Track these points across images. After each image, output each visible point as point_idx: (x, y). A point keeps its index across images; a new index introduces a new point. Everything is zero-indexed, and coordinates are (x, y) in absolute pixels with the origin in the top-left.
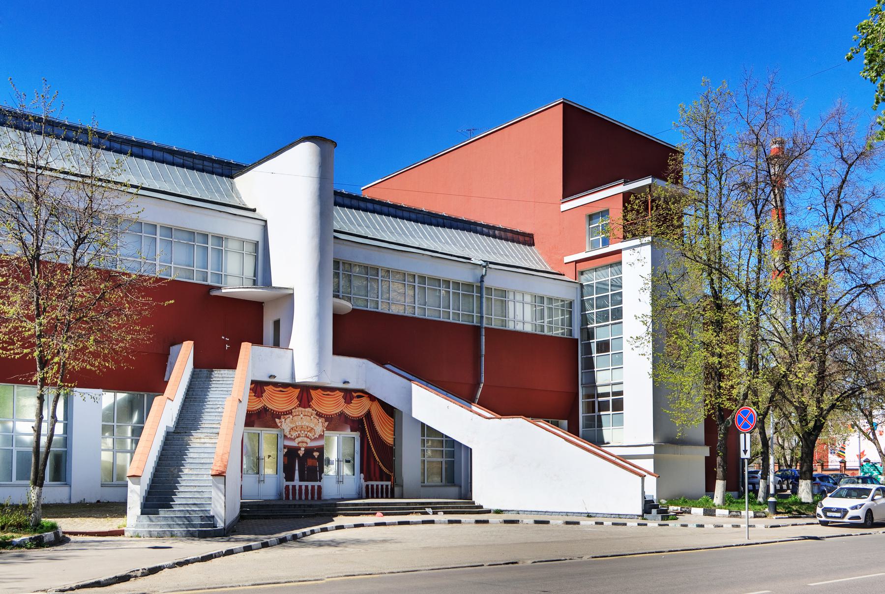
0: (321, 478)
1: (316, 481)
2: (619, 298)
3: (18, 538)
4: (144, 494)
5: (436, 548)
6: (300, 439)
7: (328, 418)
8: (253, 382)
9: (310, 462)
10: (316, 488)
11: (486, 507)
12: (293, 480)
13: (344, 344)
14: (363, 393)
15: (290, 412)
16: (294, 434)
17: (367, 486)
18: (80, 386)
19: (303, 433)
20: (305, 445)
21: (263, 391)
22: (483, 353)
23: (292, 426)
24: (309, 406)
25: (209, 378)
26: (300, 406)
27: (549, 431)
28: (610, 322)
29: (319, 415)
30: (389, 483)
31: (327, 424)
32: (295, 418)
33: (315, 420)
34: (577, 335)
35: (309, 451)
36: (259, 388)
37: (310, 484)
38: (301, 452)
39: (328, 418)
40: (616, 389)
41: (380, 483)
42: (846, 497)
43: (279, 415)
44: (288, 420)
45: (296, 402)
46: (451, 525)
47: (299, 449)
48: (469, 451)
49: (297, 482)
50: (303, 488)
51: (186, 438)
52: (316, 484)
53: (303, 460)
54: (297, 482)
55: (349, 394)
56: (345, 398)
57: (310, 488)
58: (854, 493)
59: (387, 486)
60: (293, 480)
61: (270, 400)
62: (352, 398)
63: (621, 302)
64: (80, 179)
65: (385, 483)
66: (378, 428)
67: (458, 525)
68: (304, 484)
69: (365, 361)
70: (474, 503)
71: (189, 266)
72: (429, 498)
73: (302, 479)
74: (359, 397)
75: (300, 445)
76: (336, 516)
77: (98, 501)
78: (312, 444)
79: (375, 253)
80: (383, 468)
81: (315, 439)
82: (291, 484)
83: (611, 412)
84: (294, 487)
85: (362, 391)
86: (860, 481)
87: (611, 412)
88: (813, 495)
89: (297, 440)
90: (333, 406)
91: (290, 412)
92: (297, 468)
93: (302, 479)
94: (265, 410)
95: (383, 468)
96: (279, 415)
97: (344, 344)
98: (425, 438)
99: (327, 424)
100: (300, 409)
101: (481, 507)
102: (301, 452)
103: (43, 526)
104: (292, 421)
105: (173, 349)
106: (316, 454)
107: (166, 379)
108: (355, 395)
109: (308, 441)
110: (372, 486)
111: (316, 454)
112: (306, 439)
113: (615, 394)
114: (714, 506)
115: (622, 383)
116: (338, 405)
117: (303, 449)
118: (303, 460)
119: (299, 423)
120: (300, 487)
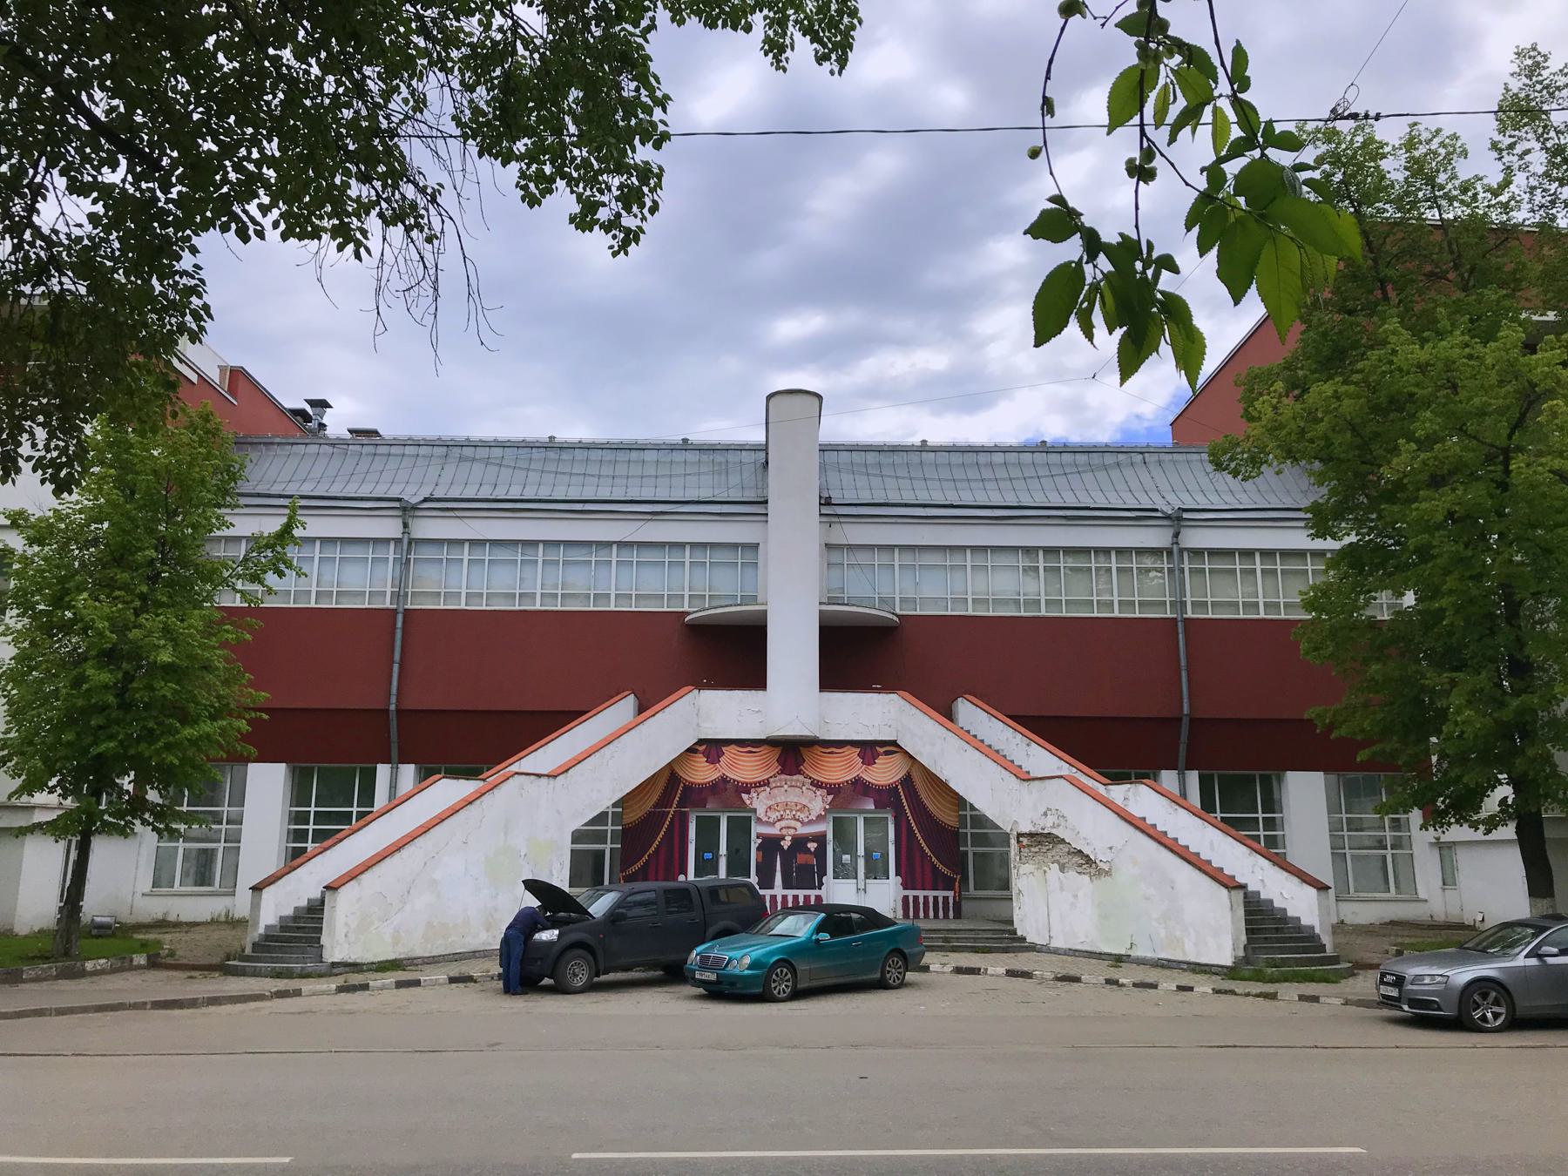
0: (821, 884)
2: (783, 988)
4: (289, 912)
6: (783, 824)
8: (509, 990)
9: (801, 858)
14: (892, 747)
15: (766, 783)
16: (774, 816)
20: (792, 832)
23: (770, 803)
24: (799, 772)
25: (1280, 780)
26: (783, 772)
29: (817, 785)
30: (950, 894)
34: (10, 638)
35: (800, 842)
36: (713, 751)
43: (747, 788)
46: (403, 991)
49: (778, 890)
51: (203, 358)
53: (788, 856)
54: (778, 890)
55: (869, 750)
58: (1490, 1013)
59: (946, 899)
62: (875, 756)
64: (1155, 537)
65: (941, 894)
66: (931, 807)
67: (414, 990)
68: (790, 893)
70: (1015, 932)
71: (983, 855)
72: (391, 676)
74: (887, 753)
75: (784, 832)
78: (803, 830)
79: (994, 904)
80: (938, 865)
81: (811, 822)
84: (774, 898)
85: (894, 743)
88: (636, 63)
89: (779, 825)
90: (840, 770)
91: (766, 783)
92: (221, 1160)
95: (938, 865)
96: (747, 788)
101: (1023, 939)
102: (786, 844)
103: (1291, 455)
106: (812, 846)
107: (194, 378)
108: (881, 750)
109: (798, 825)
111: (812, 846)
112: (793, 823)
116: (851, 767)
117: (789, 838)
118: (788, 856)
120: (785, 898)
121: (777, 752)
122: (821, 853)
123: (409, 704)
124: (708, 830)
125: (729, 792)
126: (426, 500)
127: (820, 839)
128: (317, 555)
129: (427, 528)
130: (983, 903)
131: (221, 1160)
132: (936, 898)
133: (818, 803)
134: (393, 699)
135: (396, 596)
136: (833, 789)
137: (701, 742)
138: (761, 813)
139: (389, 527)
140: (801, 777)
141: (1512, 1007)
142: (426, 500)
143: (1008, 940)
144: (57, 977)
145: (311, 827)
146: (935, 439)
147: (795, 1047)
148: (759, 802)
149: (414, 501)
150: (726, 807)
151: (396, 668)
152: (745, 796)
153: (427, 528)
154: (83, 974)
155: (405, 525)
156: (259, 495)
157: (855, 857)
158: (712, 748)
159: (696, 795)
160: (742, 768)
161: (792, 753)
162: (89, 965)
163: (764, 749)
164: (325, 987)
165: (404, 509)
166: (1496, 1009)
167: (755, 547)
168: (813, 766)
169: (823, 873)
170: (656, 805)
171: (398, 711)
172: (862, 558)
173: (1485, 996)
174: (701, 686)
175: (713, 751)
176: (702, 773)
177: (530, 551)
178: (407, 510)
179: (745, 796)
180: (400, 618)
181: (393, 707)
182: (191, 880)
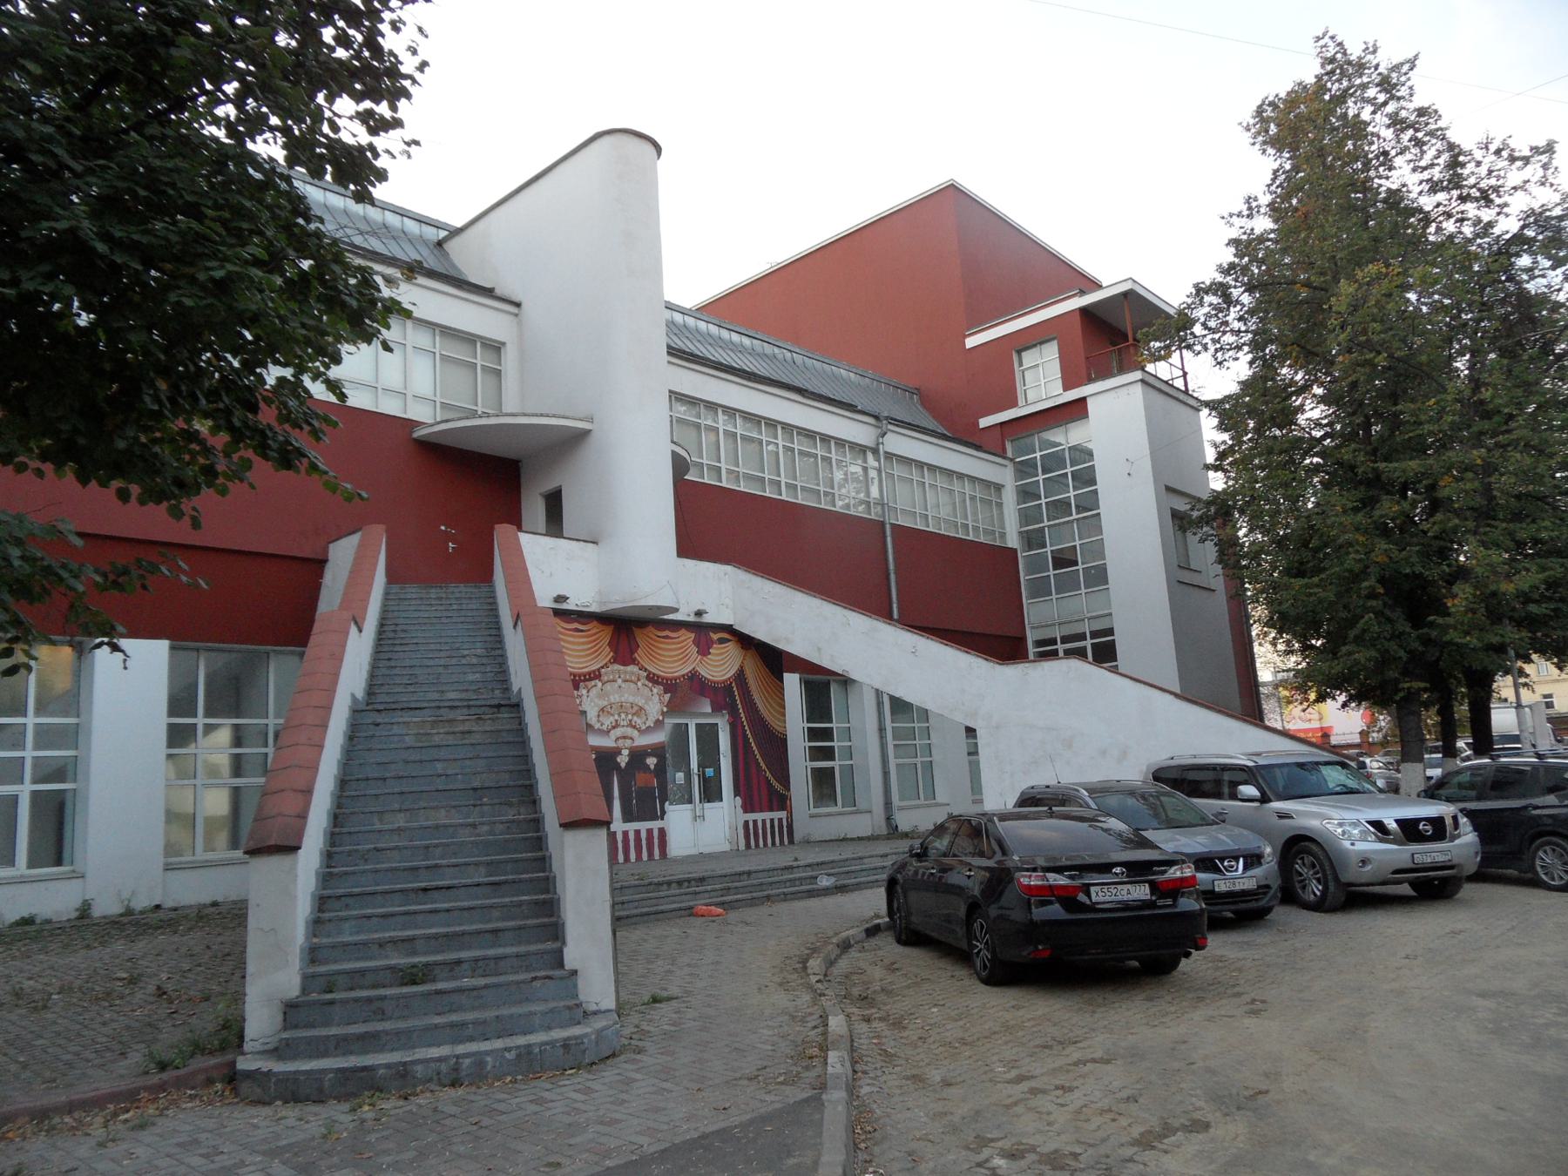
1: (654, 817)
5: (869, 839)
6: (618, 732)
7: (669, 686)
11: (459, 225)
13: (692, 543)
15: (596, 675)
16: (608, 721)
17: (746, 823)
19: (624, 719)
20: (628, 743)
22: (892, 567)
24: (633, 661)
26: (615, 660)
27: (1218, 756)
28: (1075, 516)
29: (653, 679)
30: (783, 815)
31: (667, 697)
32: (608, 687)
33: (646, 691)
37: (643, 826)
39: (669, 686)
40: (1098, 626)
41: (767, 815)
42: (613, 916)
44: (594, 692)
45: (607, 654)
47: (618, 752)
48: (952, 193)
50: (632, 836)
52: (655, 825)
55: (704, 632)
56: (697, 642)
57: (644, 835)
63: (1093, 482)
69: (729, 568)
74: (721, 641)
75: (620, 743)
77: (129, 912)
80: (773, 781)
85: (728, 629)
87: (1083, 591)
90: (677, 658)
91: (596, 675)
95: (773, 781)
97: (692, 543)
99: (667, 697)
100: (617, 667)
102: (623, 760)
105: (331, 546)
108: (715, 637)
111: (651, 762)
112: (630, 731)
113: (1094, 634)
114: (1316, 380)
117: (625, 752)
119: (615, 698)
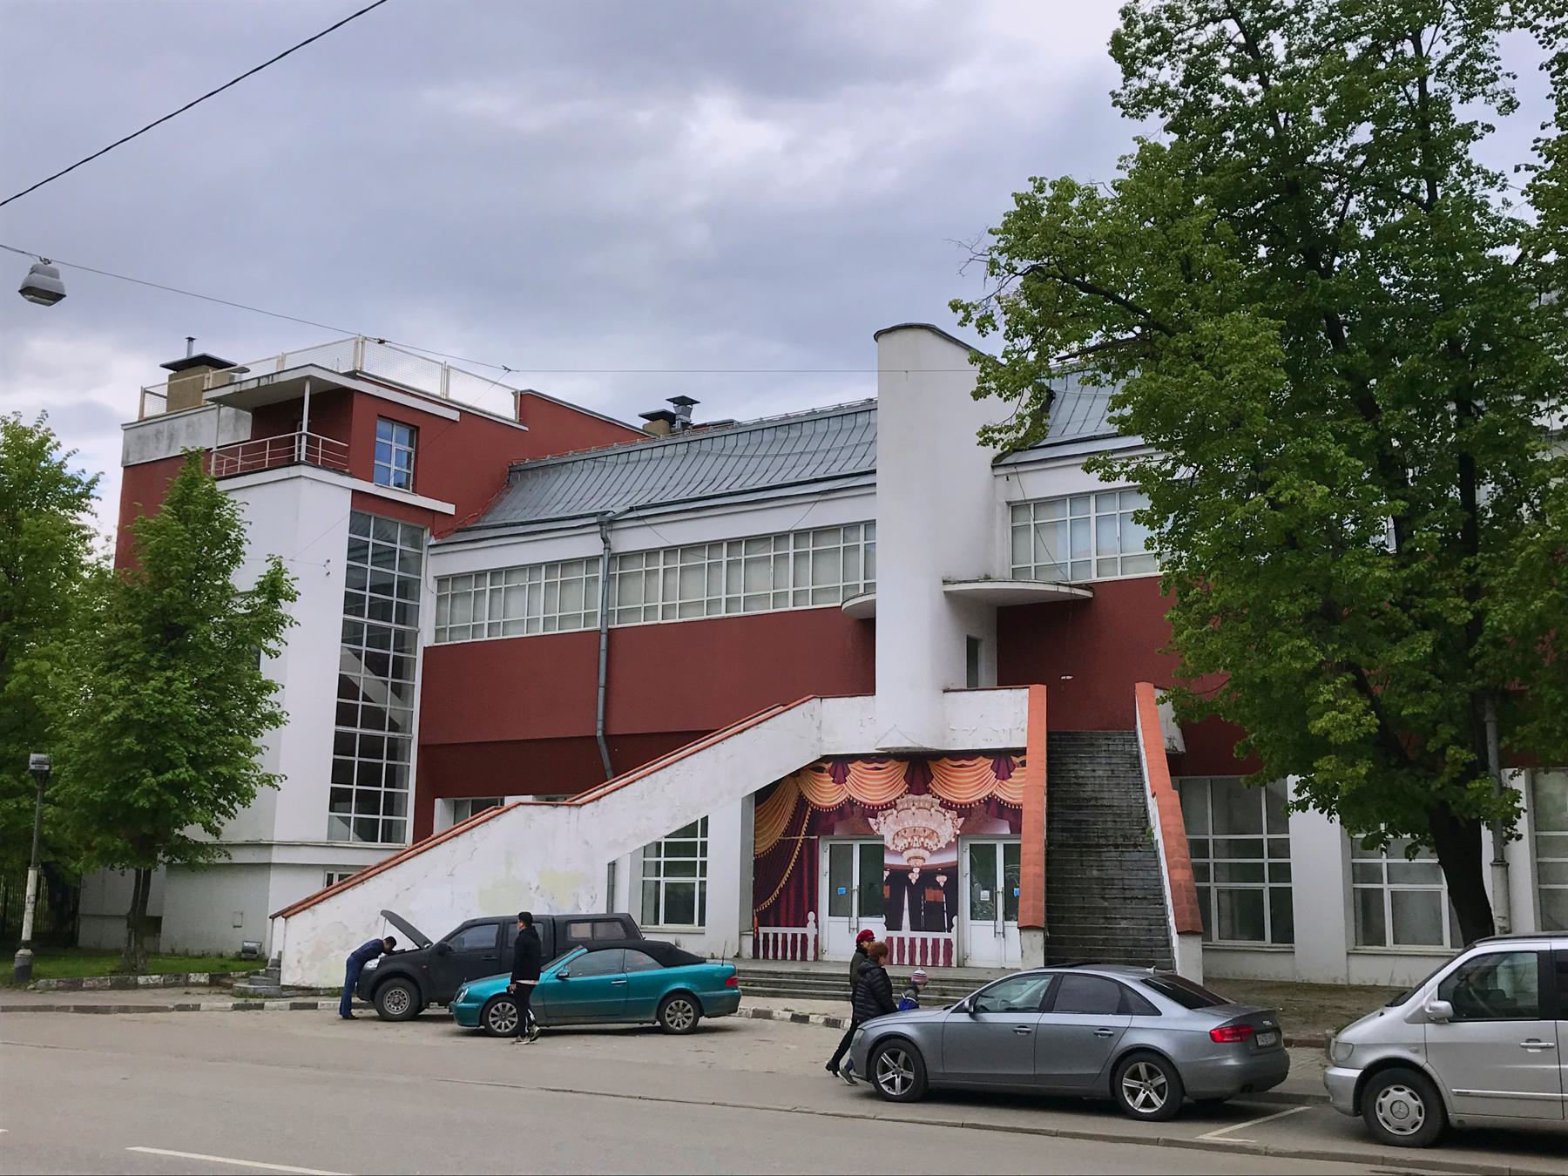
0: (951, 925)
1: (942, 930)
2: (506, 1025)
3: (1293, 1020)
6: (911, 853)
9: (930, 895)
10: (942, 943)
12: (899, 929)
15: (892, 805)
16: (901, 843)
18: (1048, 942)
19: (916, 842)
20: (920, 863)
21: (846, 772)
24: (928, 791)
26: (909, 791)
29: (947, 805)
35: (928, 875)
36: (1003, 763)
37: (930, 936)
38: (914, 877)
43: (873, 811)
44: (890, 819)
49: (906, 932)
54: (906, 932)
60: (899, 929)
61: (858, 787)
63: (339, 736)
68: (919, 935)
73: (915, 927)
75: (912, 863)
76: (1349, 825)
79: (1249, 958)
81: (940, 851)
82: (895, 934)
83: (664, 841)
86: (842, 890)
89: (907, 854)
90: (971, 786)
91: (892, 805)
93: (915, 927)
94: (851, 802)
96: (873, 811)
98: (698, 859)
100: (911, 796)
102: (914, 877)
104: (898, 820)
106: (942, 880)
107: (455, 416)
109: (926, 854)
110: (923, 964)
111: (942, 880)
112: (922, 852)
115: (874, 472)
116: (983, 783)
117: (917, 870)
118: (917, 891)
119: (909, 823)
121: (903, 768)
122: (952, 888)
123: (616, 730)
124: (840, 858)
125: (856, 815)
126: (631, 510)
127: (952, 871)
128: (1093, 515)
129: (629, 540)
130: (1236, 956)
131: (203, 1157)
132: (924, 941)
133: (947, 827)
134: (600, 725)
135: (607, 615)
136: (964, 811)
137: (826, 759)
138: (888, 841)
139: (591, 545)
140: (928, 797)
141: (922, 1072)
142: (631, 510)
143: (78, 948)
144: (112, 988)
145: (1266, 861)
146: (745, 414)
147: (214, 1060)
148: (886, 827)
149: (617, 510)
150: (856, 835)
151: (601, 691)
152: (871, 820)
153: (629, 540)
154: (136, 986)
155: (605, 541)
156: (506, 525)
157: (993, 896)
158: (838, 765)
159: (823, 821)
160: (869, 787)
161: (919, 768)
162: (141, 980)
163: (890, 765)
164: (221, 1005)
165: (601, 524)
166: (1154, 1097)
167: (870, 524)
168: (945, 785)
169: (954, 910)
170: (784, 834)
171: (606, 737)
172: (1065, 513)
173: (1152, 1073)
174: (824, 694)
175: (1003, 763)
176: (827, 794)
177: (1079, 506)
178: (607, 523)
179: (871, 820)
180: (604, 638)
181: (599, 733)
182: (1360, 941)
